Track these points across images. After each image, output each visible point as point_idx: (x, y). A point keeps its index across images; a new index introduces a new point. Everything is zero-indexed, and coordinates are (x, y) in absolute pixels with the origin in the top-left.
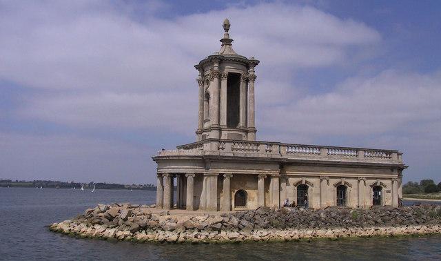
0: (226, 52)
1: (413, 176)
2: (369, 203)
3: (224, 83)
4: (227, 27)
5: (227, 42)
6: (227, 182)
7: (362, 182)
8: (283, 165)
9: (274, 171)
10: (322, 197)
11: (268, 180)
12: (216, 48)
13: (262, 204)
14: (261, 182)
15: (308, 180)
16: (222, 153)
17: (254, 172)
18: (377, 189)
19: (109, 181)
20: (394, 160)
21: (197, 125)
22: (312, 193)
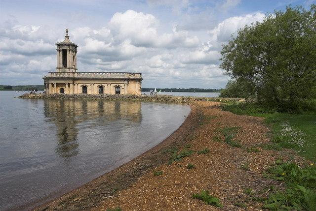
0: (67, 42)
1: (145, 85)
2: (113, 93)
3: (61, 53)
4: (67, 32)
5: (67, 37)
6: (55, 85)
7: (109, 85)
8: (74, 79)
9: (71, 82)
10: (93, 90)
11: (69, 84)
12: (62, 40)
13: (56, 92)
14: (67, 85)
15: (119, 85)
16: (53, 76)
17: (64, 82)
18: (118, 87)
19: (201, 88)
20: (137, 76)
21: (208, 97)
22: (89, 88)
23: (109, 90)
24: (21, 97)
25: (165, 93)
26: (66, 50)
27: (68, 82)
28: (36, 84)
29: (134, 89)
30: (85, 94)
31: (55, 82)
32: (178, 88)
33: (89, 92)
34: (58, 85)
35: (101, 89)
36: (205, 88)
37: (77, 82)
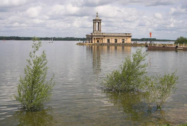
1: (132, 38)
2: (121, 42)
8: (105, 36)
9: (103, 37)
11: (102, 39)
22: (118, 40)
23: (112, 41)
24: (77, 44)
25: (65, 101)
26: (97, 21)
27: (102, 37)
28: (2, 36)
29: (129, 41)
30: (116, 43)
31: (95, 37)
32: (57, 37)
33: (118, 42)
34: (97, 38)
35: (116, 41)
36: (75, 37)
37: (105, 37)
